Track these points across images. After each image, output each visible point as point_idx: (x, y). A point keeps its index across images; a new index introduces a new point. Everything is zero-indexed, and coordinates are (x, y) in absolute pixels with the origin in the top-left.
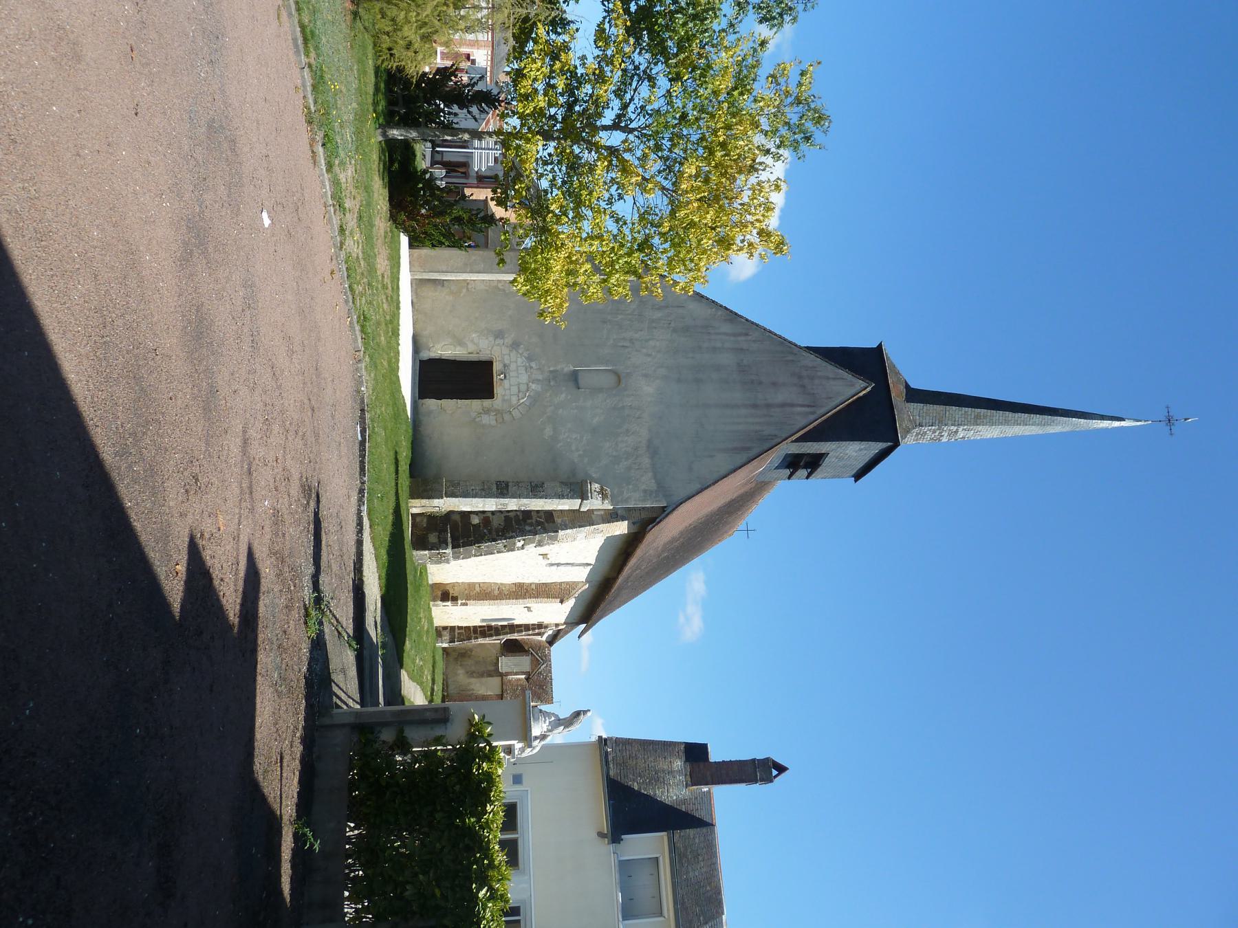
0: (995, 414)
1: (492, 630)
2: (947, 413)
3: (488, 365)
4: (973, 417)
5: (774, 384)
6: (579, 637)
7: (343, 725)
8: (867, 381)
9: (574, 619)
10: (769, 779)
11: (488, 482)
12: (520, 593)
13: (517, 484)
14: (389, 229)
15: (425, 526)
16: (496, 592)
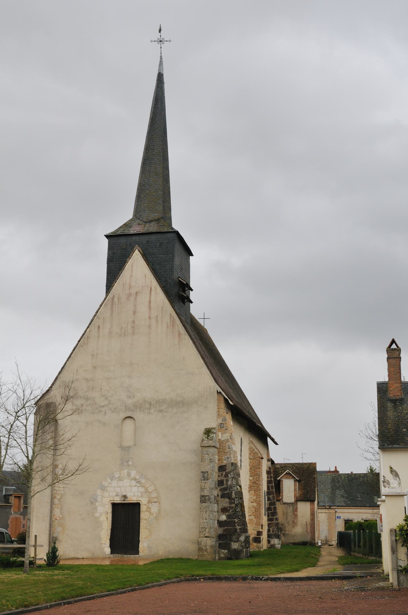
1: (271, 507)
2: (153, 194)
3: (137, 505)
5: (135, 313)
6: (276, 444)
7: (398, 578)
8: (134, 250)
9: (266, 448)
10: (398, 350)
11: (200, 509)
12: (256, 488)
13: (202, 489)
14: (125, 564)
15: (227, 551)
16: (255, 504)
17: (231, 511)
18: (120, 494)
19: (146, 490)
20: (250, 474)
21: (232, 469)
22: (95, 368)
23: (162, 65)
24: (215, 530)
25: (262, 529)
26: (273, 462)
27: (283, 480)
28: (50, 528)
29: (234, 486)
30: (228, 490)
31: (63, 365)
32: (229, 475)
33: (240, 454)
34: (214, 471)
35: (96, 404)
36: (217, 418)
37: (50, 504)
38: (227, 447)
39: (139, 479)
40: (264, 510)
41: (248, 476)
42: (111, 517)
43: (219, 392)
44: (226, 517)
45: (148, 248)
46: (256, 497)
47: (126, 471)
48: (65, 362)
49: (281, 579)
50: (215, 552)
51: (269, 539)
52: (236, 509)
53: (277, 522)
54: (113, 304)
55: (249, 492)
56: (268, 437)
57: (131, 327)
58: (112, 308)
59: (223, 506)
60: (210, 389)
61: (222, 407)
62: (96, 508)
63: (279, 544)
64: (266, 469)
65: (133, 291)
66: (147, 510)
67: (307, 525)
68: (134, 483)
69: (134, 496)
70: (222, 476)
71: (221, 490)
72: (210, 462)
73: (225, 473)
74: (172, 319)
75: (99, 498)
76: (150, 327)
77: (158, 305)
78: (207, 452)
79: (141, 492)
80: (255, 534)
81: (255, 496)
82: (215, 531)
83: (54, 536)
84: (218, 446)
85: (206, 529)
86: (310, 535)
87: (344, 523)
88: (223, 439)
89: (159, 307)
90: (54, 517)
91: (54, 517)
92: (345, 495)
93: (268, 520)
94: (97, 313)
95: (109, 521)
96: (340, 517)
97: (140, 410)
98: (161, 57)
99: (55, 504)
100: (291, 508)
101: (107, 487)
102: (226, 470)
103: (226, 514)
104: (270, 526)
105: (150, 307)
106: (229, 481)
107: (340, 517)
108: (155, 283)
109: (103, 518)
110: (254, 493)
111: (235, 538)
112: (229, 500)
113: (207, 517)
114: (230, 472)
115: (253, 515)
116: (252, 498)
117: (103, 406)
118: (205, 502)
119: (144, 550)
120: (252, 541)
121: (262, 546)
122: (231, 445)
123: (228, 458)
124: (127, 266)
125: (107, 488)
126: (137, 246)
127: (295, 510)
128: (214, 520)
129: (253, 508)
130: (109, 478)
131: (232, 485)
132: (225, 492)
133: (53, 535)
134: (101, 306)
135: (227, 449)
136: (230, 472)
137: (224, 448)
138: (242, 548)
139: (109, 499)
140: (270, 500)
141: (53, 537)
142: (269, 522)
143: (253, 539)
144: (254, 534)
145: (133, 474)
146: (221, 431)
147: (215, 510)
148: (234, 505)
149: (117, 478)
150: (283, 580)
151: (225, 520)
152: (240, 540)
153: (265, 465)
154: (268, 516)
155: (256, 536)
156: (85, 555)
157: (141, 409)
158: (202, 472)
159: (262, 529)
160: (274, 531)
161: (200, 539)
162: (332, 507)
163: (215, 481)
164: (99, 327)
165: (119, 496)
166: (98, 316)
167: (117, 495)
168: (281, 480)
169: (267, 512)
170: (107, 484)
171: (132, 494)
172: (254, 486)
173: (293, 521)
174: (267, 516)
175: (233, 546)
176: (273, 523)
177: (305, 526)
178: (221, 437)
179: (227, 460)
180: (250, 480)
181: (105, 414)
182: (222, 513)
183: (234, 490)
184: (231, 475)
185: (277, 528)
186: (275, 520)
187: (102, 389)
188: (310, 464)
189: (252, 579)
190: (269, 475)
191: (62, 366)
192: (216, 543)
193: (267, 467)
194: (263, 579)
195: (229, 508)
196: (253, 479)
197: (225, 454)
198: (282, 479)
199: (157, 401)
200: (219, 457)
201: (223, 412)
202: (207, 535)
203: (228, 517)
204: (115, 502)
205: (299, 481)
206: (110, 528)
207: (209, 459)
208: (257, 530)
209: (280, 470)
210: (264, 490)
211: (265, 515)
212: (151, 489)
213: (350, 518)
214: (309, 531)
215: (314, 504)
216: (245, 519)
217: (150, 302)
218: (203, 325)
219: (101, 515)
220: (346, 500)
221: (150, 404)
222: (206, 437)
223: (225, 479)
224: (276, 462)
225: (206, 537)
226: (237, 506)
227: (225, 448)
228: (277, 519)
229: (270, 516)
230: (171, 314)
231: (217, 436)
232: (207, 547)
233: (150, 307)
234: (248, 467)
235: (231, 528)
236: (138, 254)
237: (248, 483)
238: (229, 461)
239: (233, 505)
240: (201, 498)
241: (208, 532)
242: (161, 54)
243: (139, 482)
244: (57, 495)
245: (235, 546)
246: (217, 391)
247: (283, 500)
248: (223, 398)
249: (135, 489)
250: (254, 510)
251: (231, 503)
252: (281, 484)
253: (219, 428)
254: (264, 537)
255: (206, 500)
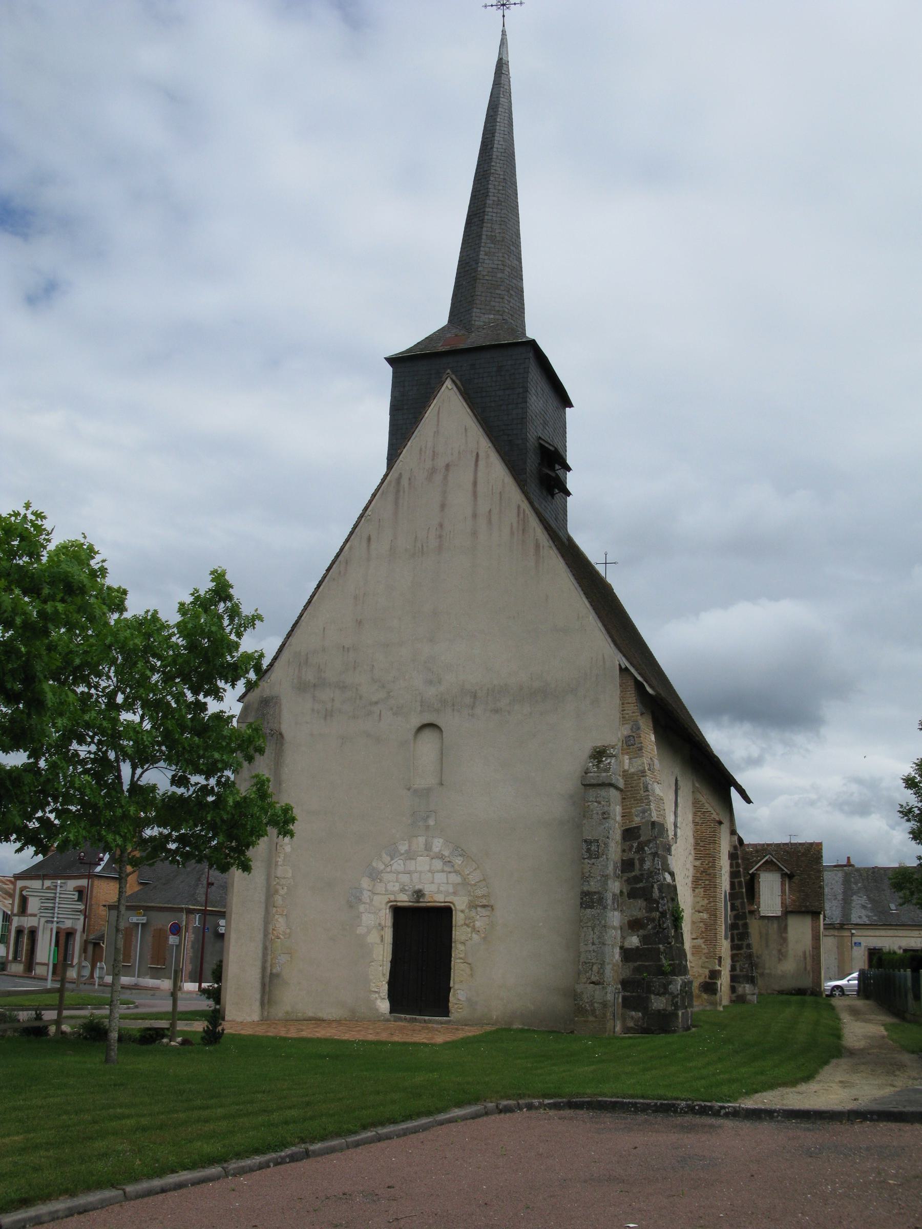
0: (489, 217)
1: (738, 924)
3: (399, 912)
4: (493, 246)
5: (443, 506)
11: (581, 921)
12: (707, 882)
13: (585, 878)
16: (705, 916)
17: (650, 927)
18: (410, 888)
19: (465, 879)
20: (696, 854)
21: (654, 835)
22: (360, 623)
23: (505, 46)
24: (615, 968)
25: (720, 965)
26: (741, 841)
27: (759, 874)
28: (265, 955)
29: (658, 872)
30: (644, 881)
31: (296, 619)
32: (646, 848)
33: (673, 810)
34: (612, 839)
35: (361, 698)
36: (620, 725)
37: (263, 905)
38: (642, 787)
39: (449, 857)
40: (723, 927)
41: (691, 858)
42: (392, 937)
43: (623, 667)
44: (640, 939)
45: (474, 378)
46: (707, 902)
47: (421, 840)
48: (300, 613)
49: (776, 1114)
50: (614, 1016)
51: (734, 984)
52: (661, 922)
53: (750, 951)
54: (398, 491)
55: (694, 891)
56: (732, 789)
57: (436, 535)
58: (397, 500)
59: (632, 916)
60: (604, 662)
61: (630, 701)
62: (359, 916)
63: (754, 994)
64: (728, 849)
65: (441, 463)
66: (467, 922)
67: (805, 958)
68: (438, 864)
69: (439, 892)
70: (630, 850)
71: (628, 881)
72: (604, 818)
73: (638, 843)
74: (521, 516)
75: (366, 896)
76: (474, 534)
77: (492, 490)
78: (596, 797)
79: (452, 884)
80: (706, 976)
81: (705, 899)
82: (613, 970)
83: (274, 971)
84: (621, 784)
85: (592, 966)
86: (811, 976)
87: (866, 953)
88: (632, 770)
89: (494, 491)
90: (274, 932)
91: (274, 932)
92: (870, 906)
93: (733, 948)
94: (366, 510)
95: (386, 945)
96: (860, 943)
97: (453, 710)
98: (504, 33)
99: (275, 905)
100: (775, 926)
101: (382, 872)
102: (639, 837)
103: (640, 933)
104: (736, 959)
105: (475, 494)
106: (645, 861)
107: (860, 943)
108: (484, 444)
109: (373, 938)
110: (703, 893)
111: (660, 986)
112: (645, 903)
113: (595, 939)
114: (649, 841)
115: (702, 938)
116: (698, 902)
117: (376, 703)
118: (592, 907)
119: (460, 1009)
120: (699, 990)
121: (721, 1001)
122: (651, 783)
123: (644, 812)
124: (428, 412)
125: (382, 875)
126: (449, 371)
127: (784, 929)
128: (612, 945)
129: (702, 923)
130: (387, 854)
131: (651, 869)
132: (638, 886)
133: (271, 970)
134: (374, 495)
135: (642, 792)
136: (649, 841)
137: (635, 790)
138: (675, 1009)
139: (385, 899)
140: (735, 910)
141: (271, 974)
142: (735, 952)
143: (702, 986)
144: (703, 977)
145: (438, 844)
146: (628, 753)
147: (615, 924)
148: (658, 913)
149: (402, 854)
150: (779, 1118)
151: (638, 947)
152: (670, 990)
153: (725, 846)
154: (732, 940)
155: (708, 980)
156: (330, 1012)
157: (455, 707)
158: (586, 841)
159: (720, 965)
160: (744, 968)
161: (579, 988)
162: (846, 927)
163: (614, 862)
164: (369, 539)
165: (407, 893)
166: (369, 517)
167: (403, 890)
168: (756, 874)
169: (729, 933)
170: (382, 867)
171: (433, 888)
172: (704, 878)
173: (780, 951)
174: (729, 940)
175: (655, 1004)
176: (740, 954)
177: (802, 959)
178: (629, 766)
179: (641, 815)
180: (695, 866)
181: (380, 719)
182: (630, 931)
183: (658, 881)
184: (650, 849)
185: (749, 964)
186: (746, 948)
187: (373, 666)
188: (811, 844)
189: (691, 1110)
190: (734, 862)
191: (294, 622)
192: (616, 996)
193: (731, 845)
194: (723, 1112)
195: (646, 921)
196: (702, 864)
197: (638, 803)
198: (759, 872)
199: (488, 690)
200: (623, 809)
201: (633, 713)
202: (594, 979)
203: (644, 939)
204: (399, 904)
205: (790, 877)
206: (390, 958)
207: (600, 812)
208: (710, 967)
209: (755, 856)
210: (723, 889)
211: (726, 938)
212: (474, 878)
213: (878, 945)
214: (809, 968)
215: (819, 918)
216: (683, 943)
217: (475, 484)
218: (603, 574)
219: (369, 932)
220: (870, 914)
221: (475, 696)
222: (594, 765)
223: (637, 857)
224: (746, 842)
225: (593, 983)
226: (665, 917)
227: (636, 790)
228: (749, 946)
229: (736, 940)
230: (519, 507)
231: (621, 763)
232: (596, 1005)
233: (475, 494)
234: (691, 840)
235: (650, 965)
236: (450, 387)
237: (691, 872)
238: (646, 819)
239: (656, 915)
240: (582, 899)
241: (598, 973)
242: (504, 26)
243: (449, 862)
244: (280, 887)
245: (658, 1003)
246: (620, 665)
247: (759, 912)
248: (633, 681)
249: (440, 878)
250: (704, 926)
251: (650, 910)
252: (756, 881)
253: (625, 747)
254: (724, 981)
255: (593, 902)
